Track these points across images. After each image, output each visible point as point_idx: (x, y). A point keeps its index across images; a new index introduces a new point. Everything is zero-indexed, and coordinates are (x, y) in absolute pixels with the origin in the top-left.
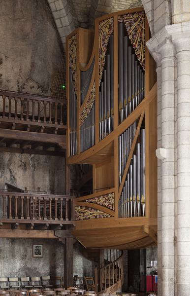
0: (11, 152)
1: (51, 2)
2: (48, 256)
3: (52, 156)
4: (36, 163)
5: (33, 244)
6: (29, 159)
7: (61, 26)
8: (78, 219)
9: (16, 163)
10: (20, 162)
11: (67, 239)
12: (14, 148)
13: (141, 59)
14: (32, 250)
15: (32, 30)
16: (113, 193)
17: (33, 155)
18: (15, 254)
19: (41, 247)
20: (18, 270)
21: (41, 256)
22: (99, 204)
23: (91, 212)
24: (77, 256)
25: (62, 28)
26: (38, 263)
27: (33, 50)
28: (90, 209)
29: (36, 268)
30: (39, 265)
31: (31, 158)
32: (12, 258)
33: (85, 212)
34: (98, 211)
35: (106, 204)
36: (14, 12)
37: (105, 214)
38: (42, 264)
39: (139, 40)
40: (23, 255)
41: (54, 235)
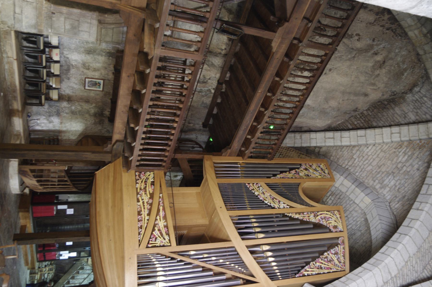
0: (223, 68)
1: (350, 134)
2: (85, 94)
3: (207, 110)
4: (203, 94)
5: (104, 80)
6: (210, 88)
7: (326, 137)
8: (137, 177)
9: (209, 73)
10: (208, 77)
11: (110, 155)
12: (226, 74)
13: (306, 271)
14: (97, 77)
15: (330, 107)
16: (170, 242)
17: (213, 91)
18: (91, 55)
19: (100, 88)
20: (68, 56)
21: (87, 88)
22: (156, 220)
23: (145, 204)
24: (84, 125)
25: (325, 137)
26: (76, 82)
27: (314, 108)
28: (150, 201)
29: (69, 79)
30: (74, 83)
31: (210, 90)
32: (85, 51)
33: (146, 191)
34: (147, 218)
35: (156, 233)
36: (350, 93)
37: (143, 231)
38: (75, 86)
39: (323, 266)
40: (89, 66)
41: (117, 141)
